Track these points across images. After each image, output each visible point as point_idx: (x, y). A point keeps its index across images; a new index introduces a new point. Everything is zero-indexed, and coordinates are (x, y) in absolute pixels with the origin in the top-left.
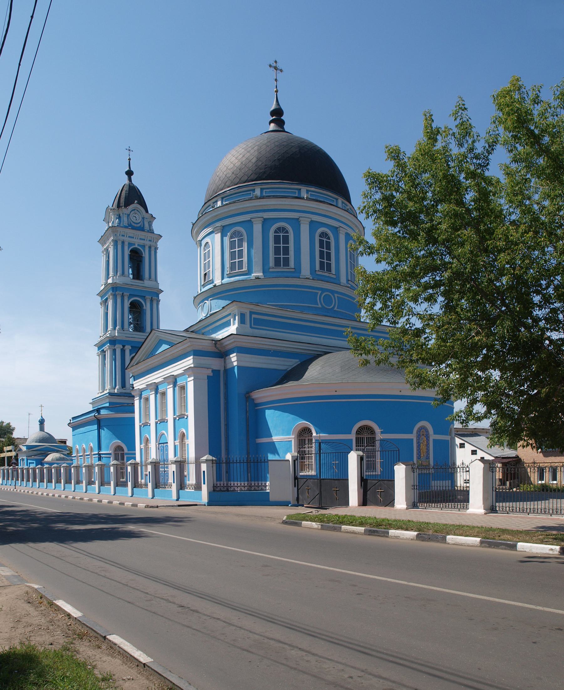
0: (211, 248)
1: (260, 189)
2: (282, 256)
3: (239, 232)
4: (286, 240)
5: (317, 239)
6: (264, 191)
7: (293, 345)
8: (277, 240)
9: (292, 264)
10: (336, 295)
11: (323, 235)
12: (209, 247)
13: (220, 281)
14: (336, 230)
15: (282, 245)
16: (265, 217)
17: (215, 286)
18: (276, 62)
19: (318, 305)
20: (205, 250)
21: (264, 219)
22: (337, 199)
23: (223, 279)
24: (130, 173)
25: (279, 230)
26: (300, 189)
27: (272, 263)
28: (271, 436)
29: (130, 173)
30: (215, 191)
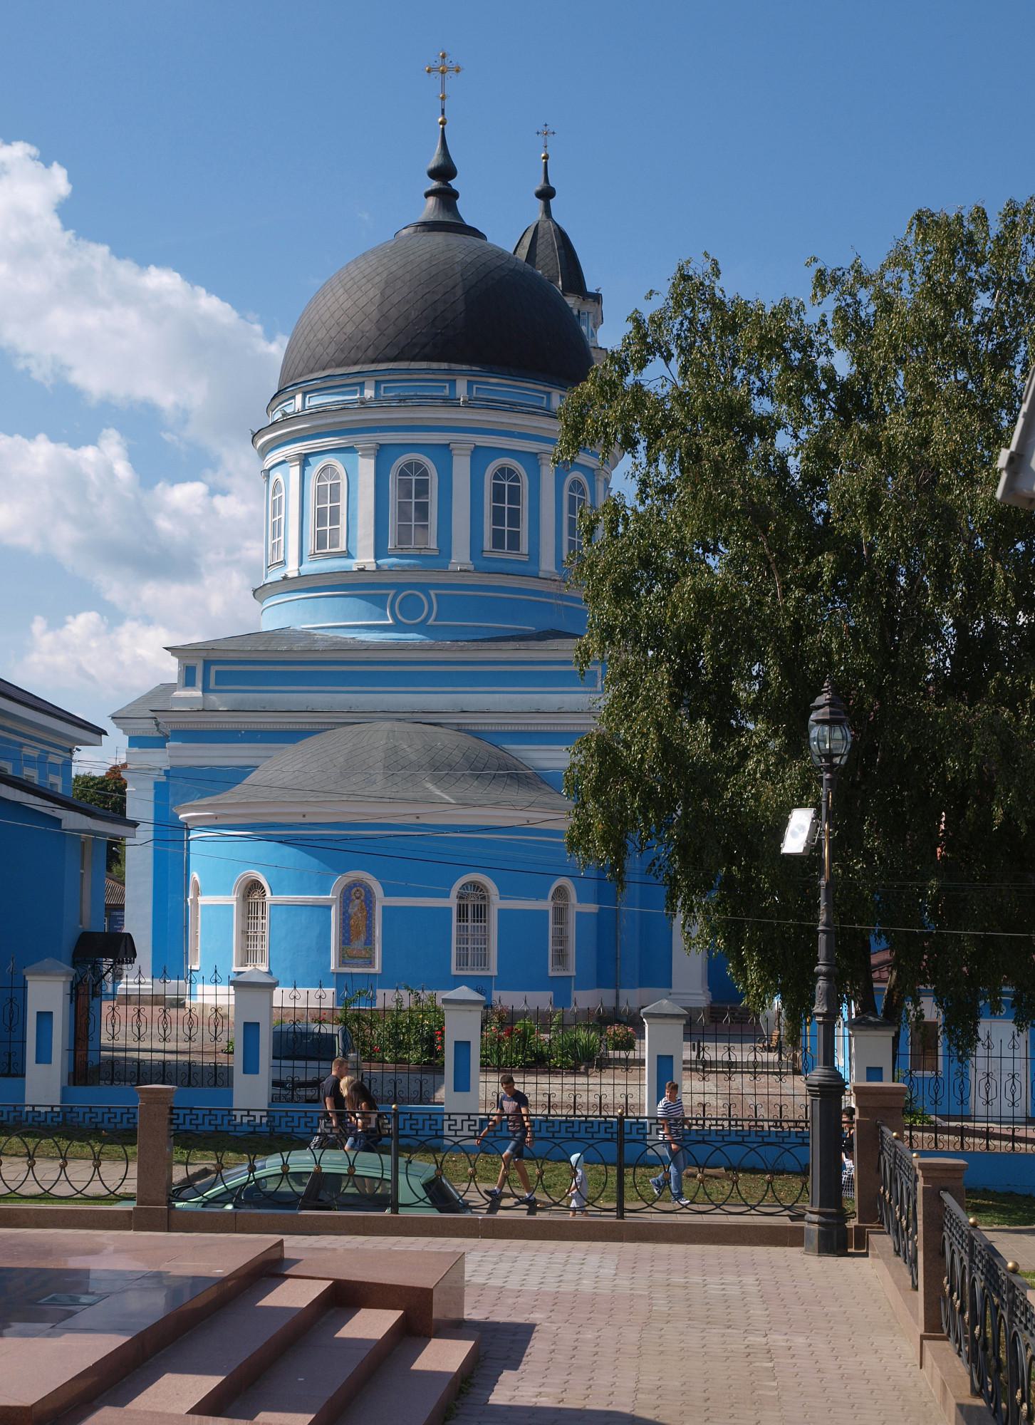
0: (283, 494)
1: (373, 382)
2: (506, 528)
3: (511, 472)
4: (515, 495)
5: (566, 493)
6: (383, 386)
7: (497, 718)
8: (498, 494)
9: (524, 547)
10: (432, 593)
11: (576, 485)
12: (281, 492)
13: (297, 567)
14: (532, 460)
15: (506, 506)
16: (478, 444)
17: (285, 578)
18: (554, 133)
19: (436, 595)
20: (274, 494)
21: (476, 447)
22: (549, 394)
23: (301, 563)
24: (546, 194)
25: (503, 472)
26: (550, 393)
27: (487, 544)
28: (819, 1230)
29: (546, 194)
30: (291, 374)
